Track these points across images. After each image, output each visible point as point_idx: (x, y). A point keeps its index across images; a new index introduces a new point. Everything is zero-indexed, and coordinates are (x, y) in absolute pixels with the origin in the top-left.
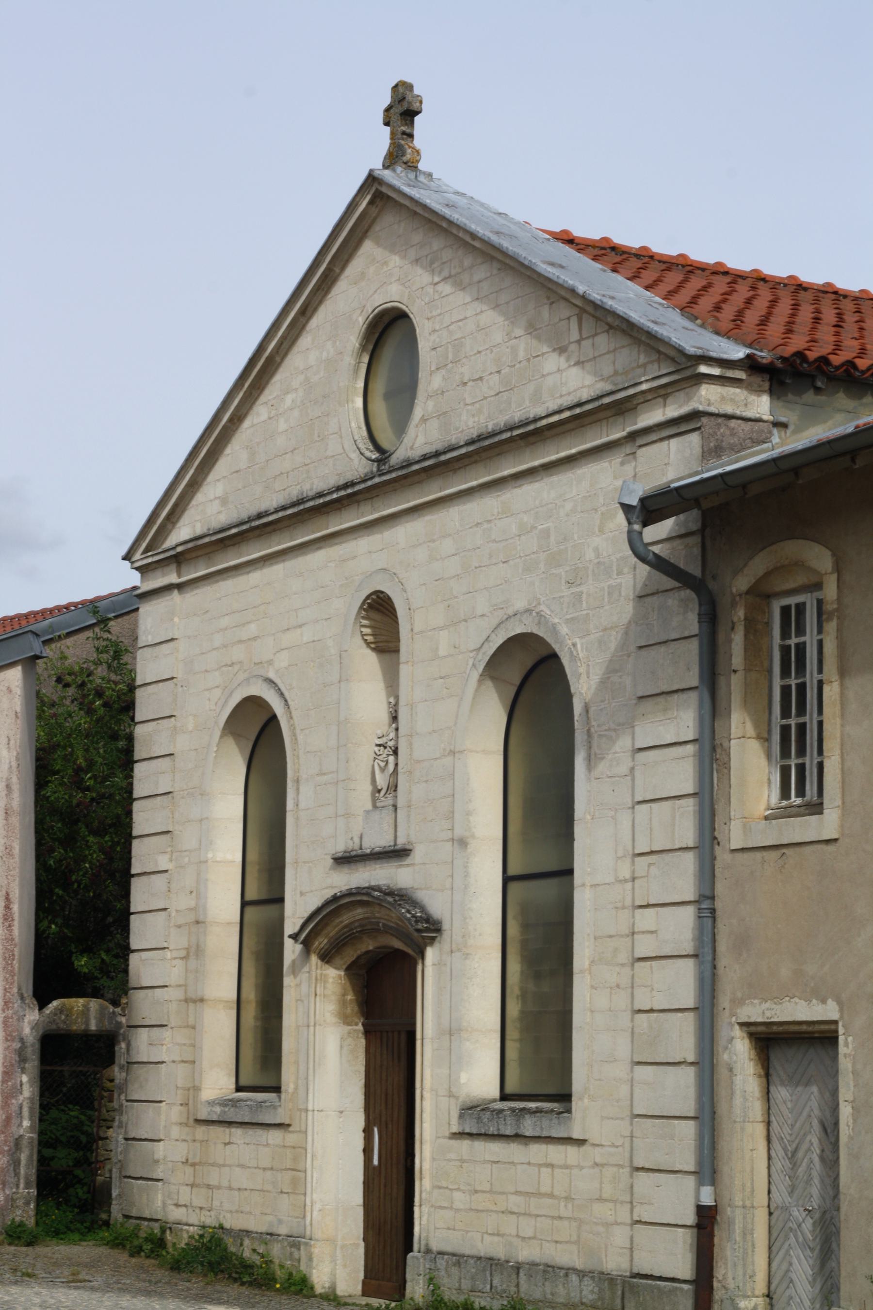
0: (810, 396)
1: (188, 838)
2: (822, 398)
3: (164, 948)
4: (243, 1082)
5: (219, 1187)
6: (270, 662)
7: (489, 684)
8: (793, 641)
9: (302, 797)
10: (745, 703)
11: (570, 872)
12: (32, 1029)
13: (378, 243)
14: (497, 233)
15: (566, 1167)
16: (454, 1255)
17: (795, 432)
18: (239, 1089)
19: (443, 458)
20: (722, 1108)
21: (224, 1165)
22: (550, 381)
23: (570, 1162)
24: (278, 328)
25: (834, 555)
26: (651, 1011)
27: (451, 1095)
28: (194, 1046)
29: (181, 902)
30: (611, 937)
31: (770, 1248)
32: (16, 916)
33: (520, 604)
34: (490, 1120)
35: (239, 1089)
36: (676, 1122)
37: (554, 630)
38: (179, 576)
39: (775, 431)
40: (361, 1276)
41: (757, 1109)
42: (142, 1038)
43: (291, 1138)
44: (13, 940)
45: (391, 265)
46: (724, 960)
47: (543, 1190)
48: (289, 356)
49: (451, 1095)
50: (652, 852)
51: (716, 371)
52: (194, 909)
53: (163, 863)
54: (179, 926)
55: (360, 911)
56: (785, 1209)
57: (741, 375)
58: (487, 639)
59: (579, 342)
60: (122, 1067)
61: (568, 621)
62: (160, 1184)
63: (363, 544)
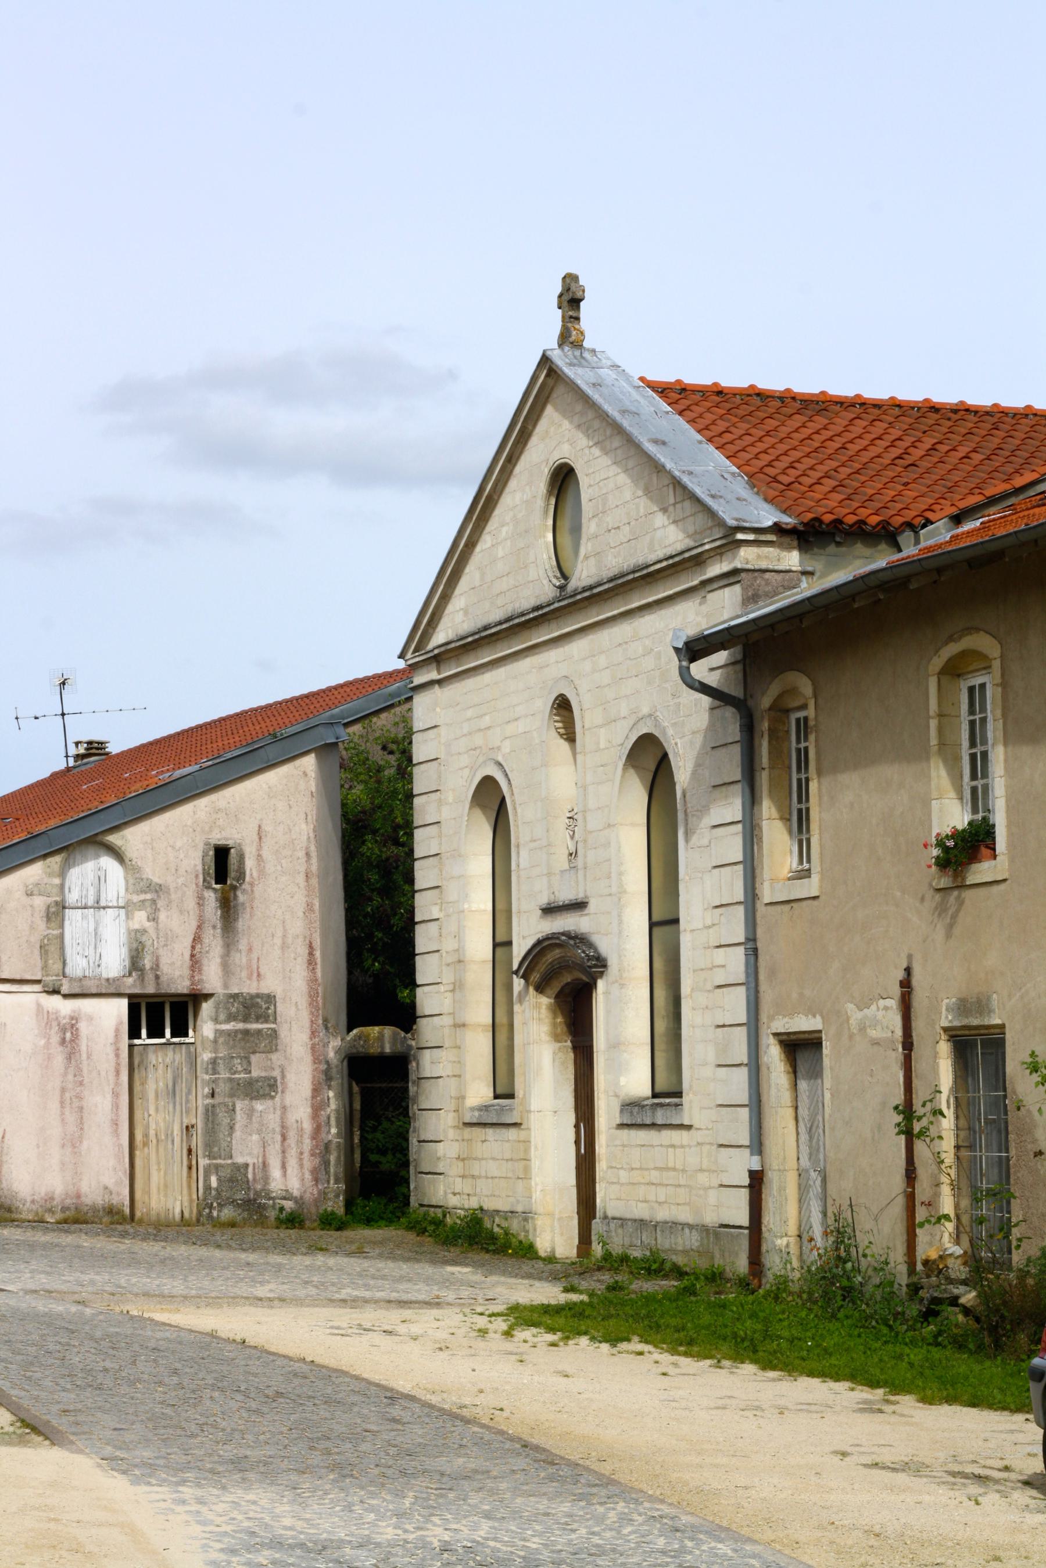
0: (832, 548)
1: (452, 892)
2: (843, 549)
3: (438, 983)
4: (499, 1091)
5: (479, 1177)
6: (499, 748)
7: (632, 772)
8: (802, 745)
9: (521, 860)
10: (771, 796)
11: (676, 921)
12: (336, 1053)
13: (556, 409)
14: (624, 412)
15: (682, 1147)
16: (621, 1219)
17: (820, 577)
18: (496, 1097)
19: (595, 591)
20: (764, 1098)
21: (483, 1159)
22: (659, 534)
23: (685, 1143)
24: (492, 474)
25: (813, 684)
26: (724, 1026)
27: (617, 1096)
28: (459, 1062)
29: (449, 945)
30: (702, 970)
31: (800, 1201)
32: (319, 961)
33: (645, 710)
34: (638, 1113)
35: (496, 1097)
36: (739, 1109)
37: (664, 731)
38: (439, 673)
39: (804, 578)
40: (576, 1241)
41: (787, 1097)
42: (427, 1056)
43: (522, 1134)
44: (316, 980)
45: (564, 428)
46: (763, 987)
47: (671, 1165)
48: (504, 495)
49: (617, 1096)
50: (722, 906)
51: (751, 537)
52: (457, 950)
53: (435, 913)
54: (448, 965)
55: (557, 951)
56: (807, 1171)
57: (772, 537)
58: (627, 737)
59: (674, 505)
60: (414, 1082)
61: (674, 725)
62: (441, 1177)
63: (552, 655)
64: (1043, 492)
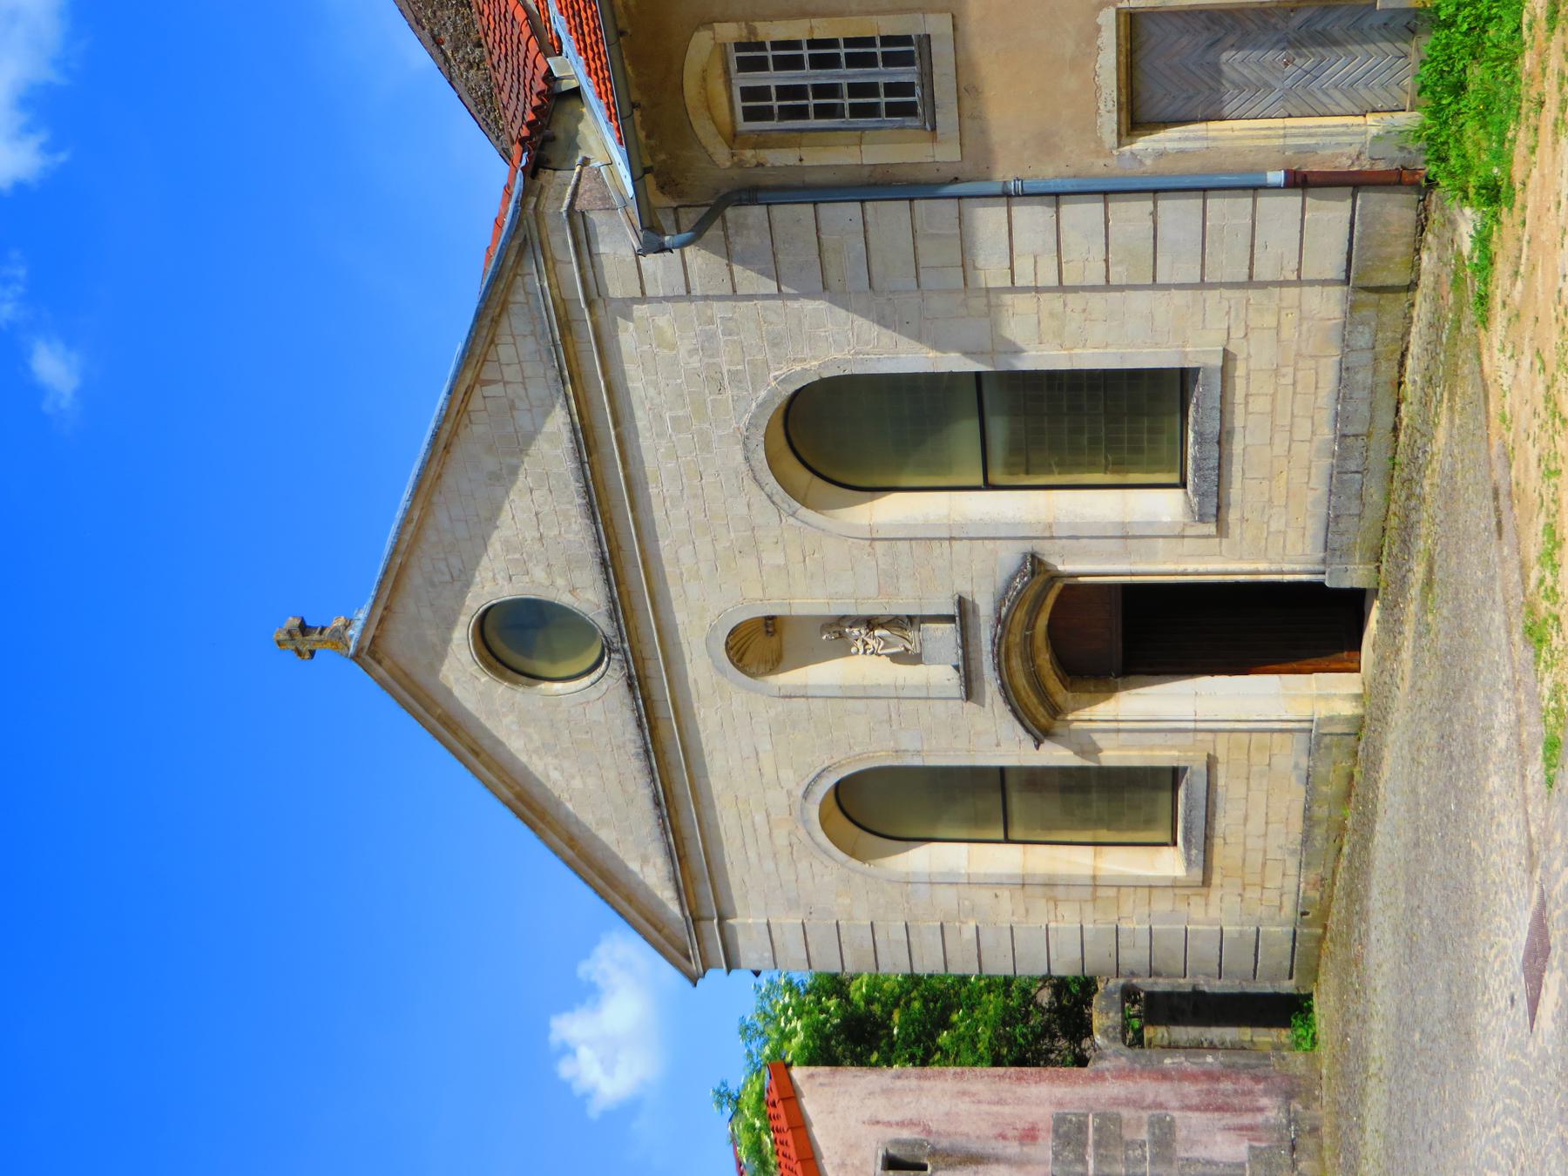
64: (537, 2)
